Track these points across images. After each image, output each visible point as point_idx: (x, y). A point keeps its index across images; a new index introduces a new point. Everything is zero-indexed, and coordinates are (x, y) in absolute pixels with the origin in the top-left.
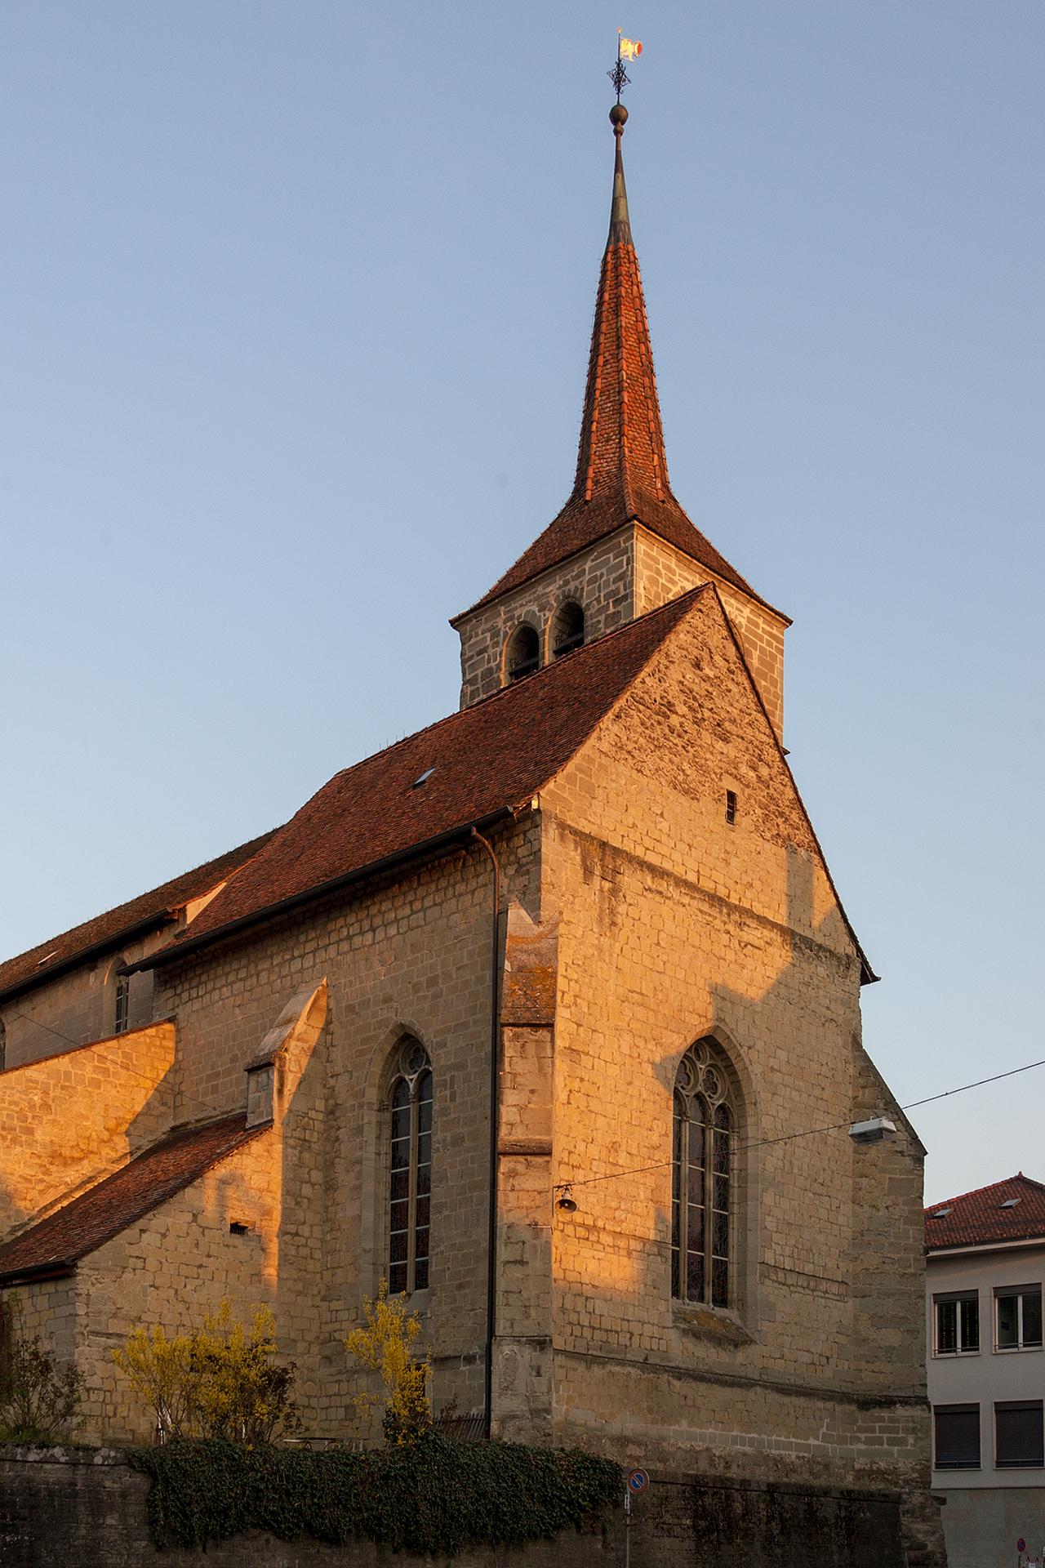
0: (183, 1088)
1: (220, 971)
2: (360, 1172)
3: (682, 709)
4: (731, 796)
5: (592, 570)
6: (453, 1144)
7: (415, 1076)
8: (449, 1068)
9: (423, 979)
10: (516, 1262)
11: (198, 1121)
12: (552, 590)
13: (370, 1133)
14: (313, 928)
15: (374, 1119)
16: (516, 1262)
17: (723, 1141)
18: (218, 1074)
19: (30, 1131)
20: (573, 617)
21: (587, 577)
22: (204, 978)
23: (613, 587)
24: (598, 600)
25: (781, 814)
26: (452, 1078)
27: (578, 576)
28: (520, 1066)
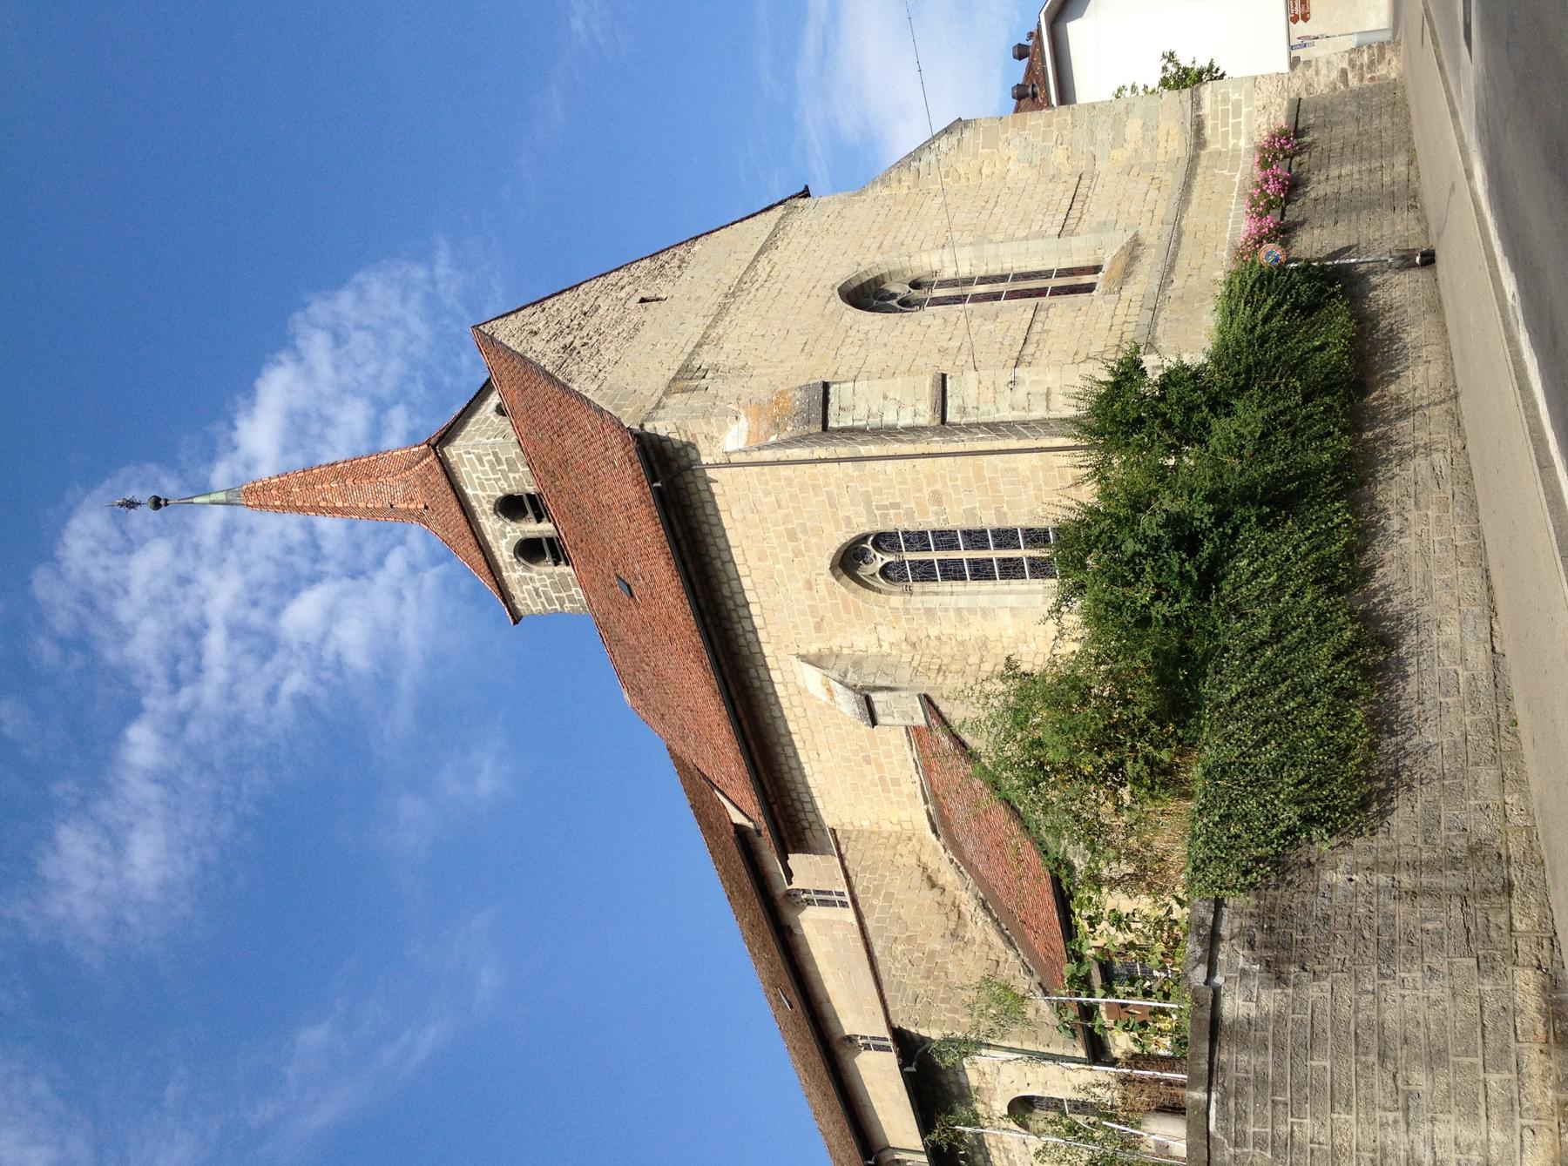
0: (895, 820)
1: (787, 777)
2: (969, 610)
3: (570, 339)
4: (643, 300)
5: (474, 488)
6: (940, 503)
7: (879, 555)
8: (870, 513)
9: (790, 545)
10: (1048, 400)
11: (926, 802)
12: (490, 524)
13: (933, 602)
15: (919, 598)
16: (1048, 400)
18: (881, 778)
19: (932, 954)
20: (511, 507)
21: (480, 492)
22: (794, 795)
23: (487, 467)
24: (497, 480)
26: (878, 508)
27: (479, 501)
28: (861, 411)
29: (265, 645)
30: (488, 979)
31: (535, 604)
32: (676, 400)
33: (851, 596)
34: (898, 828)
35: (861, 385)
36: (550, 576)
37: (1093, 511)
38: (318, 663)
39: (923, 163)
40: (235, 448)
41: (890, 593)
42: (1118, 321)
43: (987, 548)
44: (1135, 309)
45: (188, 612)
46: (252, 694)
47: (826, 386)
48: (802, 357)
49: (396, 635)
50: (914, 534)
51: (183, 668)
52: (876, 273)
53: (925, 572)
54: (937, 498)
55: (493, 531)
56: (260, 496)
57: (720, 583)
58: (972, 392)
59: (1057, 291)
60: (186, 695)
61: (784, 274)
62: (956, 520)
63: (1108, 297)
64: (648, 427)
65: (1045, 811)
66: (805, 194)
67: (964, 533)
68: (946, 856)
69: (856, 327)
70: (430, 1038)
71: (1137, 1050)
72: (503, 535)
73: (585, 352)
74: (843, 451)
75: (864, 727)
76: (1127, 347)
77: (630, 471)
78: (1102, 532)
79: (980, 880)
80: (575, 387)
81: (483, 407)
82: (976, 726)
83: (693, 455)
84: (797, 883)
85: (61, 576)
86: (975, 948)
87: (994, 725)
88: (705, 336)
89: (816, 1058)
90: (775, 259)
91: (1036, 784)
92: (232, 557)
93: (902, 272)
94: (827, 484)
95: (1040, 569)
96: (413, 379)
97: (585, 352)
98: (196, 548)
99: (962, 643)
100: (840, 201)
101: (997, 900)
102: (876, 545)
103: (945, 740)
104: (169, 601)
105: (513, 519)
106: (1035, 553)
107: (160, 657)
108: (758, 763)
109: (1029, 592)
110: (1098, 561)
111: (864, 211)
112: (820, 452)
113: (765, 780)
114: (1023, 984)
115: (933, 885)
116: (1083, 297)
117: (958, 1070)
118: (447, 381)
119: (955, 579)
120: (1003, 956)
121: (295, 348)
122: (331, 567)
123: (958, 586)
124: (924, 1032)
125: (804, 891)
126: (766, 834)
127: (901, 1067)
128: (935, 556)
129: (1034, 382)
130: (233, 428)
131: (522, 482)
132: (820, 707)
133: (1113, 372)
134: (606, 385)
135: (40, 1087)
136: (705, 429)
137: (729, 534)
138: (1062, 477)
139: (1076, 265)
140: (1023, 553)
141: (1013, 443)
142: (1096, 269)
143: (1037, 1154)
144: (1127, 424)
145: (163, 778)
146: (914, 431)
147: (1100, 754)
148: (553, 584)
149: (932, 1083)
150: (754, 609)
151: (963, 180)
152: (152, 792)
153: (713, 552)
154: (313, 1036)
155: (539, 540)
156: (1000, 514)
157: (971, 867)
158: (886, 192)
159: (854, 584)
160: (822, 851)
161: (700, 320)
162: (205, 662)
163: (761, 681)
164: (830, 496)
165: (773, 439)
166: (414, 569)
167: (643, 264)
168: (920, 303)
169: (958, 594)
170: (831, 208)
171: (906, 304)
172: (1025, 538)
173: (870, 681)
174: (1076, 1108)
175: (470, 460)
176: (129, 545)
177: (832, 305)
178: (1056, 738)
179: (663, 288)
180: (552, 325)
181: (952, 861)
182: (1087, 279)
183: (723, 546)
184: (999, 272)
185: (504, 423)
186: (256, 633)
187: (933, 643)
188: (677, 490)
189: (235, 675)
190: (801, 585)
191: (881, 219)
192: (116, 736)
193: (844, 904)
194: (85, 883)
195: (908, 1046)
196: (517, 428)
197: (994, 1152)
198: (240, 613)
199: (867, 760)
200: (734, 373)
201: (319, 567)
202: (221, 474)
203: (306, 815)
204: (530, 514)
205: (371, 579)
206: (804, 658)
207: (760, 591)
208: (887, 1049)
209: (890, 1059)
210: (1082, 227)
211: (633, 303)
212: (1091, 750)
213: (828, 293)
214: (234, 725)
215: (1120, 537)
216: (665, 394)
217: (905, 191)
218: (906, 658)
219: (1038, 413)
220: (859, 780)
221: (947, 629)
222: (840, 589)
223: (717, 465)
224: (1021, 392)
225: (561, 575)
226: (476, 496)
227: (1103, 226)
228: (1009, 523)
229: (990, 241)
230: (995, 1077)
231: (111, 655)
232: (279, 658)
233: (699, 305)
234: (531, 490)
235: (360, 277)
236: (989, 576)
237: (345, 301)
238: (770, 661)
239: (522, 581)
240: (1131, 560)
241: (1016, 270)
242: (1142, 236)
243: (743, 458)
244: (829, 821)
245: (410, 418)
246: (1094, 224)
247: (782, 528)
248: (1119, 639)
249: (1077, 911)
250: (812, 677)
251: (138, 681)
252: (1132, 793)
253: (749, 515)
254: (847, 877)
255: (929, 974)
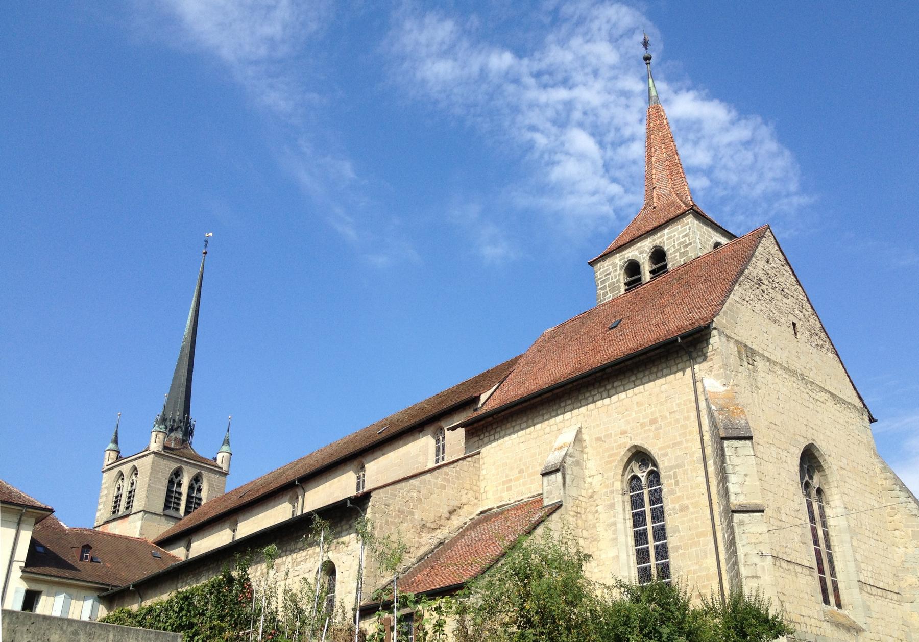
0: (487, 489)
1: (509, 425)
3: (766, 282)
4: (794, 324)
6: (681, 510)
7: (645, 474)
8: (671, 468)
9: (648, 420)
10: (753, 577)
11: (498, 507)
12: (647, 245)
13: (619, 508)
14: (569, 399)
16: (753, 577)
17: (821, 508)
18: (510, 480)
19: (412, 514)
20: (659, 255)
21: (666, 237)
22: (498, 429)
25: (817, 335)
26: (675, 473)
27: (660, 237)
28: (736, 461)
29: (562, 120)
30: (381, 261)
31: (601, 274)
32: (733, 348)
33: (619, 458)
34: (482, 491)
35: (752, 460)
36: (618, 281)
37: (685, 607)
38: (553, 152)
39: (899, 493)
40: (676, 92)
41: (622, 482)
42: (807, 620)
43: (655, 540)
44: (815, 630)
45: (578, 77)
46: (533, 117)
47: (750, 438)
48: (766, 423)
49: (572, 193)
50: (660, 495)
51: (546, 78)
52: (825, 467)
53: (636, 502)
54: (684, 509)
55: (643, 247)
56: (654, 114)
57: (621, 380)
58: (754, 529)
59: (823, 581)
60: (531, 81)
61: (818, 409)
62: (670, 521)
63: (822, 613)
64: (714, 332)
65: (500, 580)
66: (872, 420)
67: (663, 526)
68: (467, 520)
69: (789, 455)
70: (350, 233)
71: (367, 637)
72: (641, 252)
73: (759, 292)
74: (709, 450)
75: (540, 469)
76: (791, 627)
77: (686, 323)
78: (673, 613)
79: (454, 541)
80: (736, 288)
81: (718, 235)
82: (547, 536)
83: (699, 360)
84: (448, 433)
85: (593, 5)
86: (417, 539)
87: (550, 548)
88: (775, 363)
89: (351, 449)
90: (828, 404)
91: (517, 574)
92: (612, 98)
93: (827, 483)
94: (687, 441)
95: (644, 574)
96: (725, 189)
97: (759, 292)
98: (615, 78)
99: (594, 526)
100: (869, 442)
101: (444, 551)
102: (651, 472)
103: (536, 517)
104: (583, 67)
105: (651, 257)
106: (654, 571)
107: (551, 65)
108: (516, 408)
109: (629, 567)
110: (654, 610)
111: (864, 457)
112: (707, 437)
113: (506, 412)
114: (400, 568)
115: (451, 513)
116: (820, 597)
117: (350, 529)
118: (727, 209)
119: (634, 521)
120: (412, 555)
121: (739, 120)
122: (609, 153)
123: (630, 523)
124: (369, 510)
125: (443, 438)
126: (475, 415)
127: (350, 498)
128: (647, 508)
129: (763, 568)
130: (688, 90)
131: (674, 261)
132: (551, 442)
133: (775, 618)
134: (739, 306)
135: (313, 26)
136: (716, 366)
137: (652, 384)
138: (704, 587)
139: (841, 593)
140: (653, 562)
141: (723, 556)
142: (839, 605)
143: (305, 579)
144: (742, 627)
145: (483, 74)
146: (726, 494)
147: (537, 613)
148: (613, 283)
149: (345, 514)
150: (607, 401)
151: (890, 519)
152: (475, 68)
153: (640, 375)
154: (347, 169)
155: (639, 273)
156: (677, 548)
157: (462, 535)
158: (878, 470)
159: (626, 460)
160: (467, 447)
161: (785, 359)
162: (550, 90)
163: (564, 407)
164: (680, 443)
165: (713, 407)
166: (611, 200)
167: (817, 322)
168: (808, 495)
169: (625, 523)
170: (864, 436)
171: (807, 486)
172: (663, 564)
173: (568, 471)
174: (330, 601)
175: (685, 230)
176: (614, 41)
177: (801, 440)
178: (545, 586)
179: (803, 336)
180: (774, 271)
181: (465, 523)
182: (832, 599)
183: (644, 381)
184: (832, 544)
185: (709, 248)
186: (568, 116)
187: (593, 509)
188: (677, 352)
189: (543, 107)
190: (623, 428)
191: (860, 468)
192: (505, 46)
193: (437, 461)
194: (423, 38)
195: (361, 501)
196: (707, 255)
197: (304, 553)
198: (579, 106)
199: (521, 471)
200: (753, 382)
201: (609, 147)
202: (660, 87)
203: (471, 153)
204: (654, 267)
205: (603, 176)
206: (579, 432)
207: (618, 404)
208: (358, 489)
209: (352, 492)
210: (866, 596)
211: (792, 318)
212: (539, 607)
213: (809, 437)
214: (516, 110)
215: (670, 624)
216: (736, 341)
217: (880, 483)
218: (583, 493)
219: (744, 571)
220: (510, 467)
221: (603, 517)
222: (623, 451)
223: (694, 375)
224: (757, 560)
225: (619, 287)
226: (664, 235)
227: (868, 608)
228: (672, 554)
229: (851, 538)
230: (349, 553)
231: (551, 37)
232: (554, 130)
233: (794, 358)
234: (670, 266)
235: (787, 153)
236: (637, 542)
237: (772, 146)
238: (576, 412)
239: (614, 265)
240: (656, 631)
241: (834, 555)
242: (863, 634)
243: (700, 390)
244: (484, 450)
245: (703, 189)
246: (868, 603)
247: (658, 415)
248: (607, 624)
249: (444, 600)
250: (568, 436)
251: (537, 55)
252: (514, 633)
253: (664, 395)
254: (453, 462)
255: (401, 512)
